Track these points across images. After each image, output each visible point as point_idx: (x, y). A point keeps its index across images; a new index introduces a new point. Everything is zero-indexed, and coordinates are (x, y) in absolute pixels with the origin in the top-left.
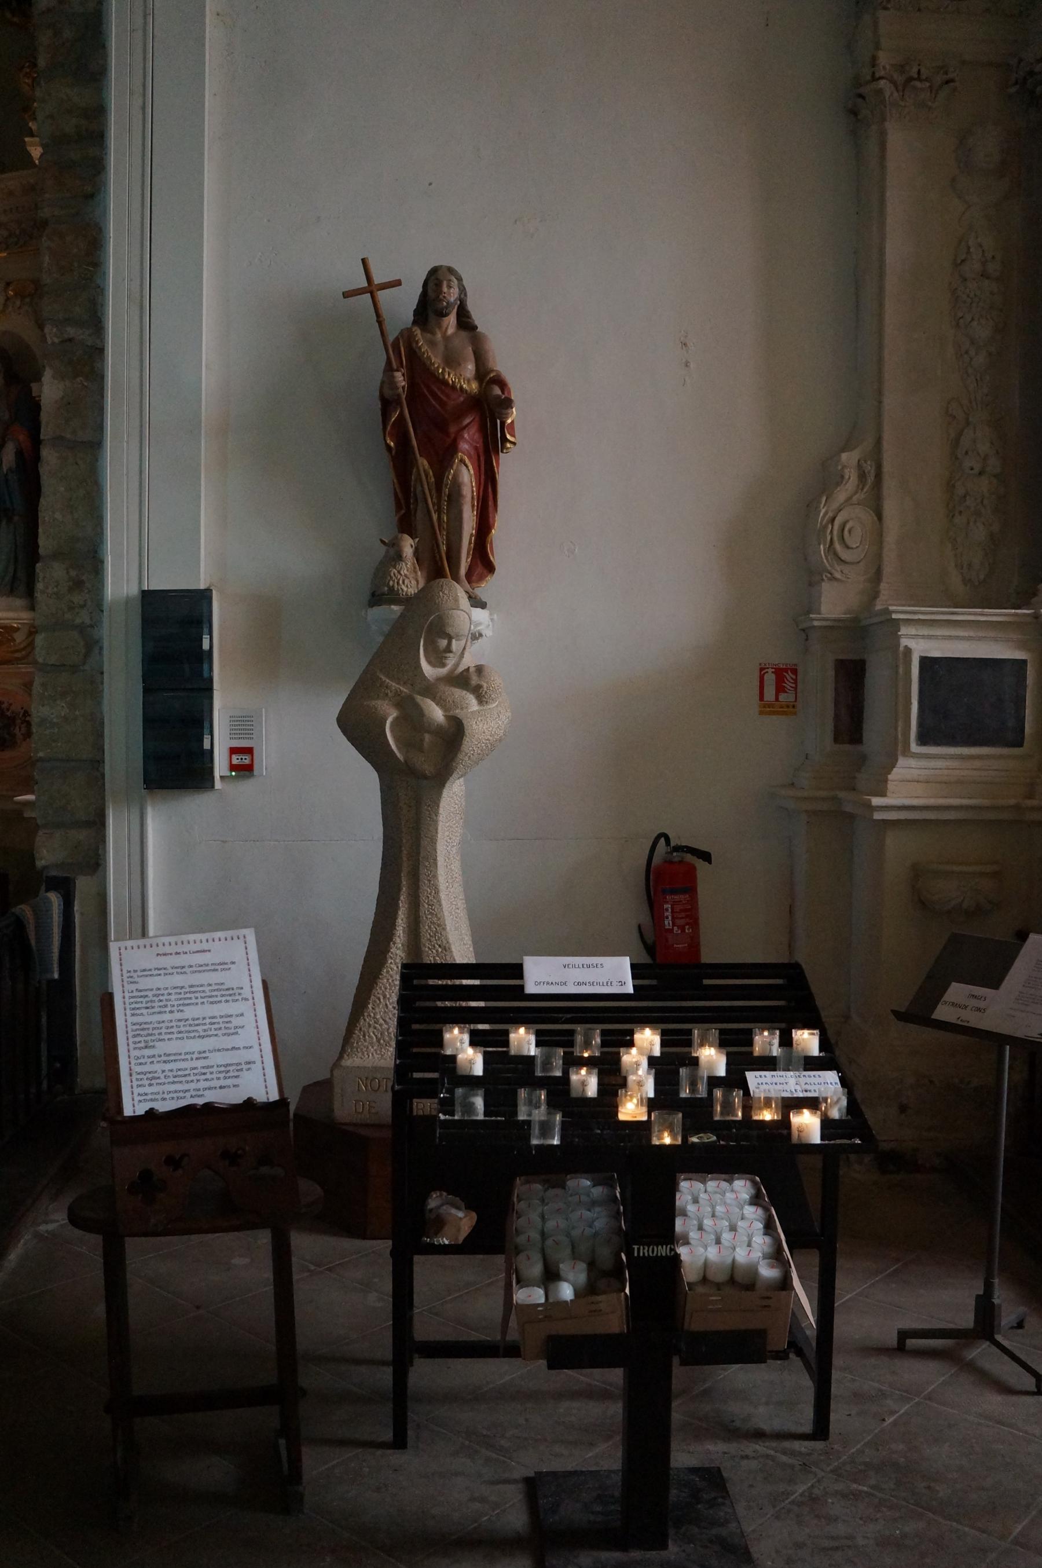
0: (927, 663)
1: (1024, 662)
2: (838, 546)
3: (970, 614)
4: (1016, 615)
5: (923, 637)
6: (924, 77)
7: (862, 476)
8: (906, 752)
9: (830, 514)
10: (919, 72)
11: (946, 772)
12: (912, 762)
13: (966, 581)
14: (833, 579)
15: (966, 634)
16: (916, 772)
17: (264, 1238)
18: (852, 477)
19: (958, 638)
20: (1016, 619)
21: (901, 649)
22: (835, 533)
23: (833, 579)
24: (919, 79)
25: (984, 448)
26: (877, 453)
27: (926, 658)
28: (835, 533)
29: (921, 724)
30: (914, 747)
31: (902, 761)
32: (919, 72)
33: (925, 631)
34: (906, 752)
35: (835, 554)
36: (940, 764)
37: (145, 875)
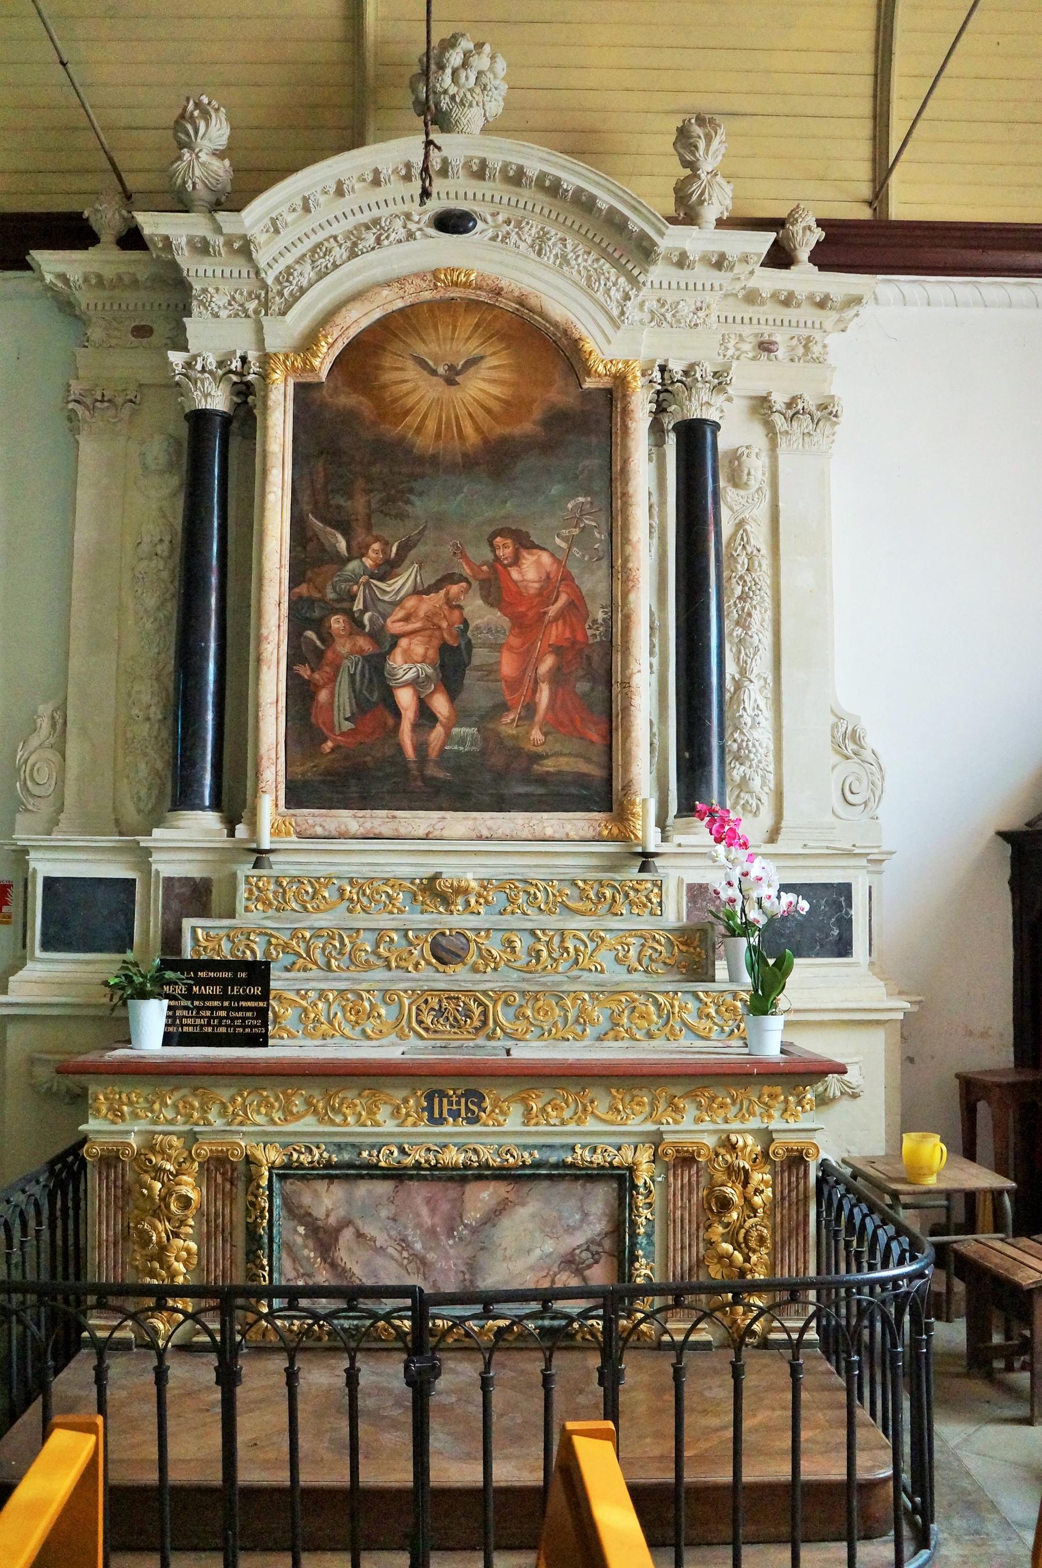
0: (50, 883)
1: (134, 880)
2: (29, 783)
3: (87, 841)
4: (122, 841)
5: (48, 860)
6: (106, 399)
7: (54, 725)
8: (33, 958)
9: (25, 756)
10: (103, 395)
11: (90, 975)
12: (39, 966)
13: (139, 811)
14: (27, 810)
15: (85, 857)
16: (38, 974)
17: (804, 1477)
18: (45, 724)
19: (78, 861)
20: (131, 844)
21: (31, 870)
22: (28, 772)
23: (27, 810)
24: (102, 401)
25: (146, 698)
26: (63, 707)
27: (49, 878)
28: (28, 772)
29: (44, 934)
30: (38, 953)
31: (30, 965)
32: (103, 395)
33: (49, 855)
34: (33, 958)
35: (28, 790)
36: (62, 967)
37: (631, 1071)
